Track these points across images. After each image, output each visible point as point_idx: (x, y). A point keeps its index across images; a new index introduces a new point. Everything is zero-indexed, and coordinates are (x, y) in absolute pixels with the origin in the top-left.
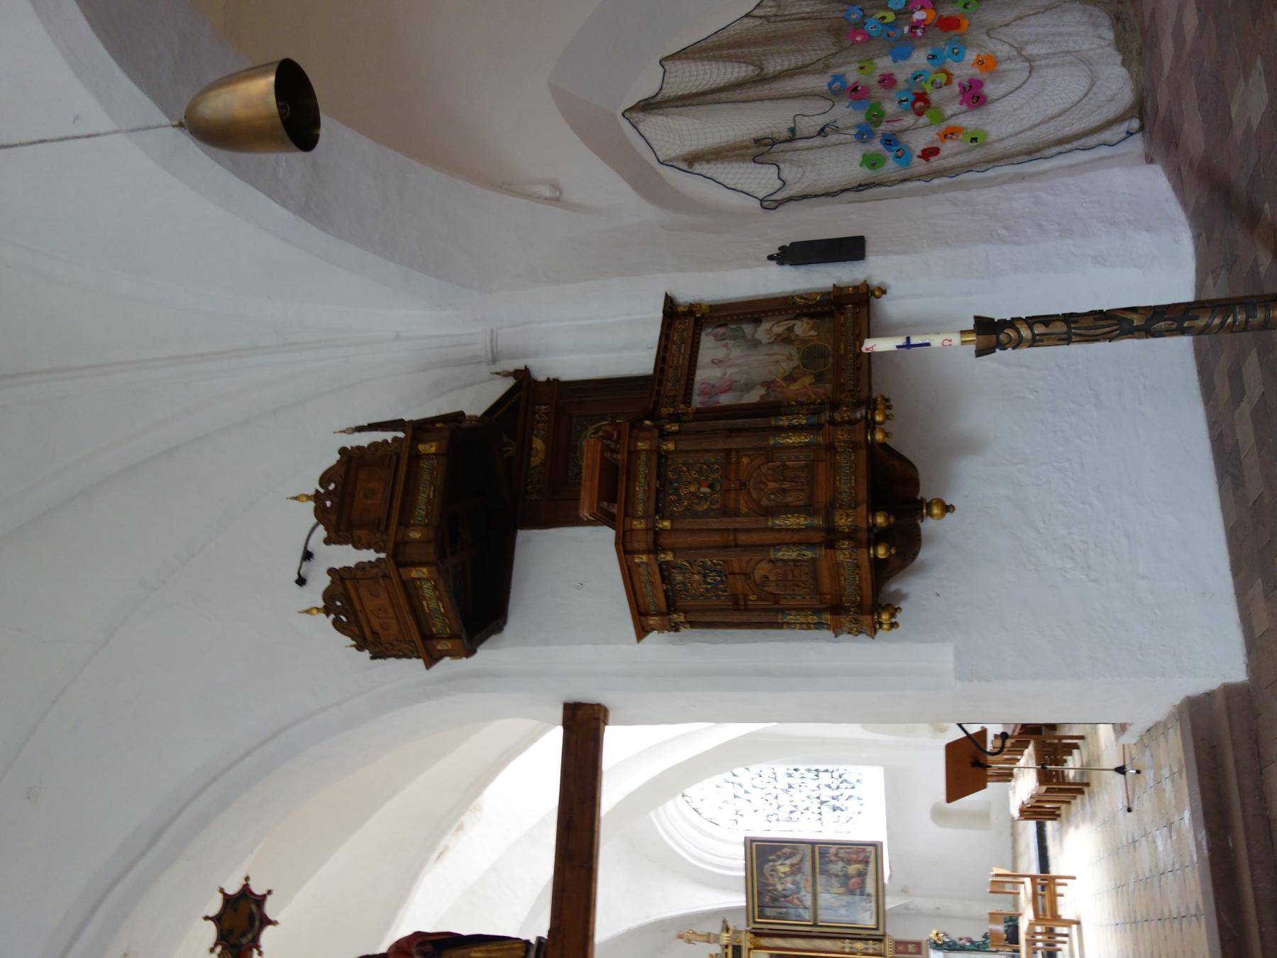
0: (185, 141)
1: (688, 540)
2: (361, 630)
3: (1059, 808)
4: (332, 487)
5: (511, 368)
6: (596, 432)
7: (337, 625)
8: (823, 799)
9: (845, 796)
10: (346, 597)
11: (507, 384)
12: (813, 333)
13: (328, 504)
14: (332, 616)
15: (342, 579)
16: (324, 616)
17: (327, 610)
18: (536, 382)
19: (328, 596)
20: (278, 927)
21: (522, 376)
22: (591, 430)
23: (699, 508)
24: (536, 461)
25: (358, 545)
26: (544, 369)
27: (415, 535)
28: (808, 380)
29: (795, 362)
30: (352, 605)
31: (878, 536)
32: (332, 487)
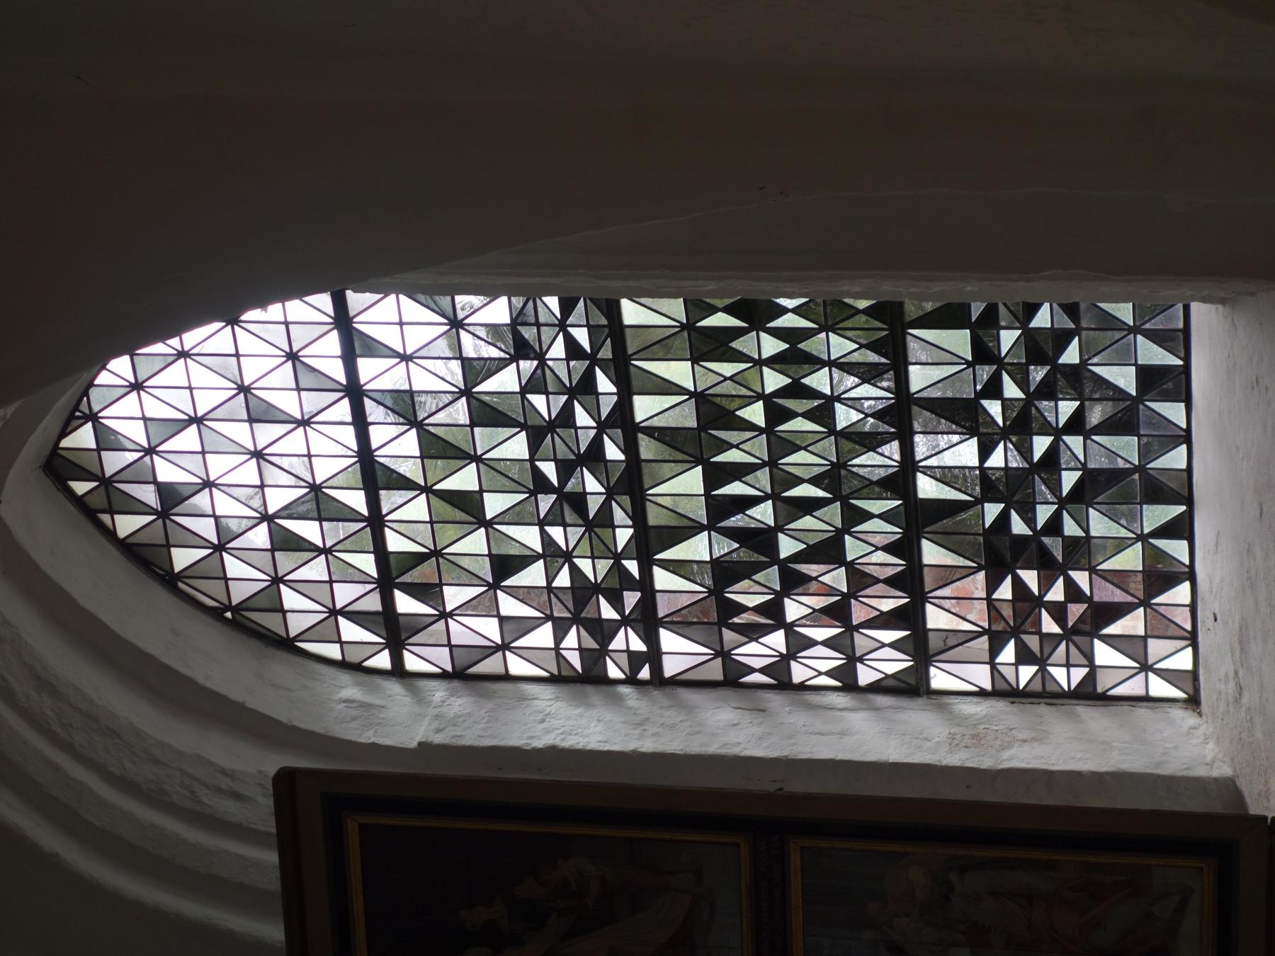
8: (927, 488)
9: (1069, 480)
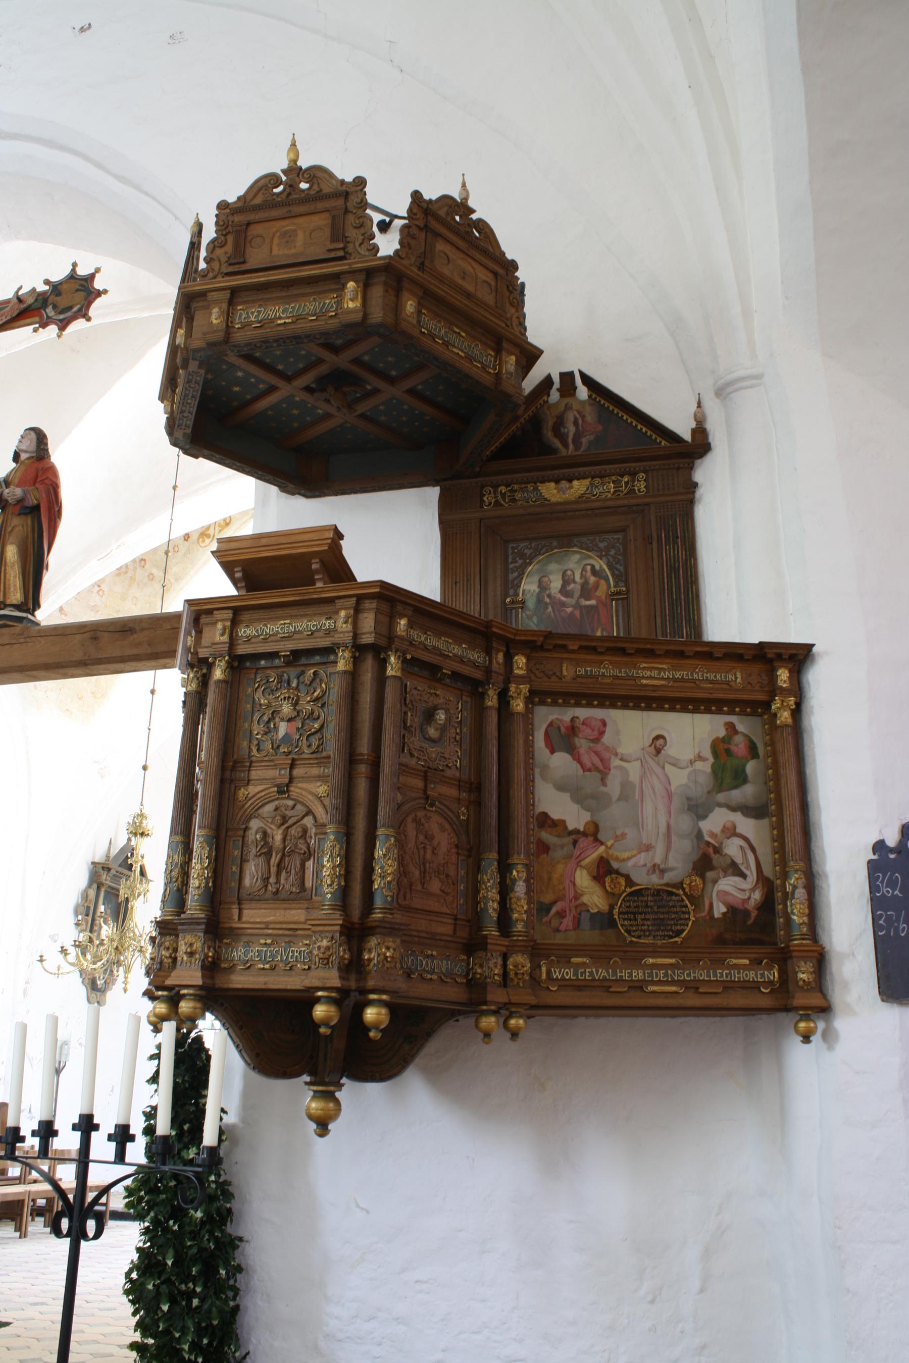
1: (366, 698)
5: (710, 426)
6: (594, 572)
7: (271, 180)
11: (683, 428)
12: (719, 909)
15: (346, 195)
16: (285, 166)
17: (294, 171)
18: (691, 468)
20: (89, 324)
21: (699, 445)
22: (600, 564)
23: (763, 990)
24: (550, 491)
26: (709, 474)
28: (595, 898)
29: (643, 879)
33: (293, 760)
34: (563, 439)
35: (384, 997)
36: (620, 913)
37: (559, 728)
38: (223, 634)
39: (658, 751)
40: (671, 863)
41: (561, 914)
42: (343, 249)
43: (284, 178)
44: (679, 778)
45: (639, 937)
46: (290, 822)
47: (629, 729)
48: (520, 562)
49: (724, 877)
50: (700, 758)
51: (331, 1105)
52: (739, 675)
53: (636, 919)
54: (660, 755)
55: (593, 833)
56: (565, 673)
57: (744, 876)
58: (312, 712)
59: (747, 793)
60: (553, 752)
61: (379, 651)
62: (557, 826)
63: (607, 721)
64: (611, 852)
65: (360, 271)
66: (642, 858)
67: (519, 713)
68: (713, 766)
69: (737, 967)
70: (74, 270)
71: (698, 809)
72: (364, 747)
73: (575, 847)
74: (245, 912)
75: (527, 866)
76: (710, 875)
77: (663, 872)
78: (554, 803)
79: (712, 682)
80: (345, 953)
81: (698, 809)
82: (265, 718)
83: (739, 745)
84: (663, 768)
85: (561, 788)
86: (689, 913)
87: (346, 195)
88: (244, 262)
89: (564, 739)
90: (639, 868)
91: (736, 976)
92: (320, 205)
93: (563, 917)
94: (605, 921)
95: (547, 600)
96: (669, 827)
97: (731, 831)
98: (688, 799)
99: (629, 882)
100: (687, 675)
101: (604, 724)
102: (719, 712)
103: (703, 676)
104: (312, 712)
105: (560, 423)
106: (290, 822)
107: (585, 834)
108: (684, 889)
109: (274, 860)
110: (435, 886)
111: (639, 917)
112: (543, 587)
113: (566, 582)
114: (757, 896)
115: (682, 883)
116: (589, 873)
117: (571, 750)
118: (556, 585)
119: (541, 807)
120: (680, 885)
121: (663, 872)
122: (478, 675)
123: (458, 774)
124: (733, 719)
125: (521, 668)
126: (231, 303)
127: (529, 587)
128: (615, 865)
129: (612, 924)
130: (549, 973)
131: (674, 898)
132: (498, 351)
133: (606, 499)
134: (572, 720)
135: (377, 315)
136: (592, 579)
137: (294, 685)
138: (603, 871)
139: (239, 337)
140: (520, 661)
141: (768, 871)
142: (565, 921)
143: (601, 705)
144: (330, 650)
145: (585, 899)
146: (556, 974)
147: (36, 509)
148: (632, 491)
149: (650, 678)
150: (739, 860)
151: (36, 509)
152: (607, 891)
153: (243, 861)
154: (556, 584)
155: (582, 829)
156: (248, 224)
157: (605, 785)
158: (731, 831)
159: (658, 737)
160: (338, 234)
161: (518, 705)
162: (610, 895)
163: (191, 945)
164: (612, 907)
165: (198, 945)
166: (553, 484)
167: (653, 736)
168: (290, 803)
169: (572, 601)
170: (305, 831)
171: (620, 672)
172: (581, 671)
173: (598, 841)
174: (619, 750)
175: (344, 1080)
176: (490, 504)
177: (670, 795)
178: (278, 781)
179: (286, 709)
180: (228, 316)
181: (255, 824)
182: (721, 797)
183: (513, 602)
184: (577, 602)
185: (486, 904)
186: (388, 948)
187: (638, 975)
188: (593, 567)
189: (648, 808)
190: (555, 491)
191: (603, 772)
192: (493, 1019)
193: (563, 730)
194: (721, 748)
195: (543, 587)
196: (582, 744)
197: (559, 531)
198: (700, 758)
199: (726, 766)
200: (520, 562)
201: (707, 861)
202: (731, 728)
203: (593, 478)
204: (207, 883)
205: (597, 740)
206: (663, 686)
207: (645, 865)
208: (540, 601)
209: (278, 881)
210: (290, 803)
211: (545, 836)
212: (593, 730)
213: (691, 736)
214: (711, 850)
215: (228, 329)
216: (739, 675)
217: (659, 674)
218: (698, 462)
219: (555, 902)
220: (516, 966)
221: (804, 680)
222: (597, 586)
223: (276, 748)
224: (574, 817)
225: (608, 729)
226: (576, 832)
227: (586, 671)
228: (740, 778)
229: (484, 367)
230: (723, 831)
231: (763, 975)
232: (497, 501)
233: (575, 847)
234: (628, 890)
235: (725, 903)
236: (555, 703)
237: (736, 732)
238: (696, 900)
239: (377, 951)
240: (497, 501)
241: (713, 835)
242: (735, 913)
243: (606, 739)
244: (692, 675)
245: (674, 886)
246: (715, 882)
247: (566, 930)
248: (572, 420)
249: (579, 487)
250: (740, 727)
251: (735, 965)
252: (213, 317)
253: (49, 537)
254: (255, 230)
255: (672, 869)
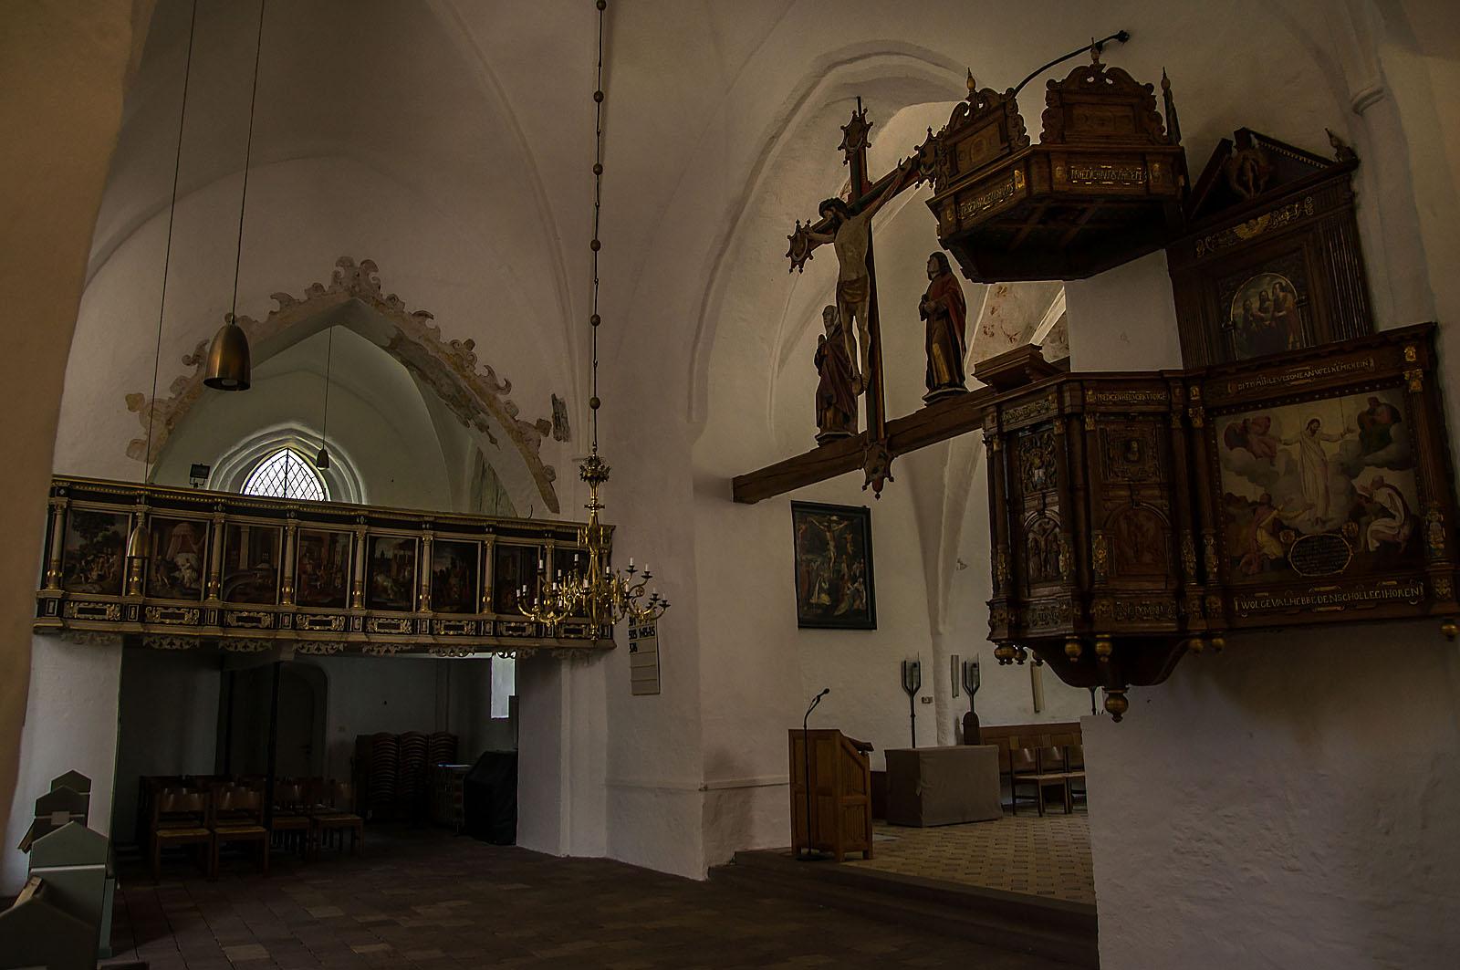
0: (735, 512)
2: (958, 132)
3: (955, 659)
4: (1109, 81)
6: (1282, 289)
10: (988, 112)
11: (1329, 153)
12: (1373, 545)
13: (1091, 80)
14: (358, 264)
15: (1004, 105)
17: (974, 96)
18: (1349, 180)
19: (987, 95)
21: (1348, 163)
22: (1284, 281)
24: (1243, 232)
25: (333, 440)
27: (1058, 172)
28: (1272, 549)
29: (1308, 530)
30: (981, 118)
31: (1087, 644)
32: (1109, 81)
33: (1043, 494)
34: (1245, 185)
35: (1106, 636)
36: (1292, 557)
37: (1235, 431)
38: (993, 422)
39: (1314, 432)
40: (1331, 514)
41: (1249, 563)
42: (1009, 146)
43: (969, 103)
44: (1332, 449)
45: (1309, 573)
46: (1049, 532)
47: (1289, 421)
48: (1228, 293)
49: (1376, 519)
50: (1349, 430)
51: (1120, 702)
52: (1372, 361)
53: (1306, 560)
54: (1316, 435)
55: (1268, 502)
56: (1230, 391)
57: (1394, 517)
58: (1050, 461)
59: (1392, 450)
60: (1231, 449)
61: (1078, 416)
62: (1241, 501)
63: (1271, 417)
64: (1281, 513)
65: (1019, 160)
66: (1306, 516)
67: (1198, 429)
68: (1360, 435)
69: (1388, 588)
70: (930, 134)
71: (1349, 471)
72: (1080, 481)
73: (1254, 514)
74: (1032, 591)
75: (1215, 536)
76: (1364, 519)
77: (1324, 523)
78: (1238, 486)
79: (1348, 371)
80: (1077, 611)
81: (1349, 471)
82: (1027, 468)
83: (1383, 415)
84: (1319, 444)
85: (1239, 473)
86: (1348, 551)
87: (1004, 105)
88: (958, 172)
89: (1239, 438)
90: (1304, 521)
91: (1386, 594)
92: (991, 118)
93: (1251, 564)
94: (1281, 564)
95: (1251, 319)
96: (1326, 487)
97: (1380, 483)
98: (1342, 464)
99: (1298, 534)
100: (1327, 370)
101: (1269, 420)
102: (1363, 391)
103: (1340, 368)
104: (1050, 461)
105: (1241, 171)
106: (1049, 532)
107: (1261, 504)
108: (1342, 533)
109: (1043, 556)
110: (1147, 558)
111: (1308, 558)
112: (1247, 309)
113: (1263, 301)
114: (1406, 530)
115: (1340, 529)
116: (1267, 531)
117: (1245, 444)
118: (1267, 296)
119: (1226, 490)
120: (1339, 530)
121: (1324, 523)
122: (1162, 409)
123: (1158, 479)
124: (1376, 394)
125: (1196, 395)
126: (957, 203)
127: (1236, 311)
128: (1285, 523)
129: (1288, 565)
130: (1239, 605)
131: (1335, 541)
132: (1145, 165)
133: (1284, 226)
134: (1245, 421)
135: (1037, 189)
136: (1281, 294)
137: (1039, 444)
138: (1277, 528)
139: (966, 225)
140: (1195, 390)
141: (1414, 510)
142: (1252, 567)
143: (1265, 407)
144: (1049, 421)
145: (1266, 550)
146: (1245, 606)
147: (946, 314)
148: (1303, 213)
149: (1296, 379)
150: (1387, 505)
151: (946, 314)
152: (1281, 542)
153: (1027, 559)
154: (1256, 304)
155: (1258, 501)
156: (955, 144)
157: (1273, 465)
158: (1380, 483)
159: (1313, 421)
160: (1005, 137)
161: (1198, 423)
162: (1286, 546)
163: (1001, 615)
164: (1286, 554)
165: (1005, 615)
166: (1244, 225)
167: (1310, 420)
168: (1047, 520)
169: (1269, 315)
170: (1056, 536)
171: (1272, 380)
172: (1241, 387)
173: (1272, 508)
174: (1282, 438)
175: (1129, 686)
176: (1201, 252)
177: (1325, 464)
178: (1039, 508)
179: (1037, 461)
180: (957, 212)
181: (1031, 536)
182: (1368, 458)
183: (1227, 326)
184: (1273, 315)
185: (1185, 565)
186: (1103, 606)
187: (1305, 601)
188: (1281, 284)
189: (843, 605)
190: (1247, 230)
191: (1271, 456)
192: (1198, 641)
193: (1238, 431)
194: (1365, 420)
195: (1247, 309)
196: (1253, 438)
197: (1252, 262)
198: (1349, 430)
199: (1371, 434)
200: (1228, 293)
201: (1360, 509)
202: (1374, 402)
203: (1272, 211)
204: (1007, 577)
205: (1264, 433)
206: (1307, 383)
207: (1309, 520)
208: (1245, 318)
209: (1046, 570)
210: (1047, 520)
211: (1232, 510)
212: (1260, 426)
213: (1338, 417)
214: (1363, 500)
215: (959, 221)
216: (1372, 361)
217: (1303, 375)
218: (1353, 173)
219: (1243, 556)
220: (1210, 604)
221: (1439, 347)
222: (1285, 297)
223: (1035, 487)
224: (1252, 492)
225: (1272, 424)
226: (1254, 503)
227: (1246, 386)
228: (1385, 440)
229: (1134, 183)
230: (1372, 485)
231: (1409, 592)
232: (1206, 249)
233: (1254, 514)
234: (1298, 539)
235: (1377, 540)
236: (1229, 413)
237: (1379, 404)
238: (1354, 540)
239: (1100, 607)
240: (1206, 249)
241: (1364, 489)
242: (1387, 546)
243: (1272, 431)
244: (1331, 370)
245: (1334, 532)
246: (1368, 524)
247: (1253, 574)
248: (1249, 167)
249: (1262, 221)
250: (1383, 400)
251: (1385, 586)
252: (948, 216)
253: (960, 330)
254: (960, 147)
255: (1332, 520)
